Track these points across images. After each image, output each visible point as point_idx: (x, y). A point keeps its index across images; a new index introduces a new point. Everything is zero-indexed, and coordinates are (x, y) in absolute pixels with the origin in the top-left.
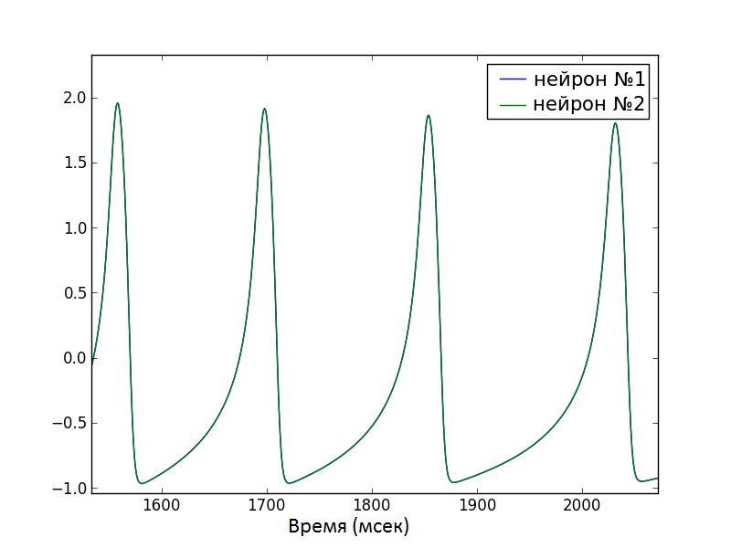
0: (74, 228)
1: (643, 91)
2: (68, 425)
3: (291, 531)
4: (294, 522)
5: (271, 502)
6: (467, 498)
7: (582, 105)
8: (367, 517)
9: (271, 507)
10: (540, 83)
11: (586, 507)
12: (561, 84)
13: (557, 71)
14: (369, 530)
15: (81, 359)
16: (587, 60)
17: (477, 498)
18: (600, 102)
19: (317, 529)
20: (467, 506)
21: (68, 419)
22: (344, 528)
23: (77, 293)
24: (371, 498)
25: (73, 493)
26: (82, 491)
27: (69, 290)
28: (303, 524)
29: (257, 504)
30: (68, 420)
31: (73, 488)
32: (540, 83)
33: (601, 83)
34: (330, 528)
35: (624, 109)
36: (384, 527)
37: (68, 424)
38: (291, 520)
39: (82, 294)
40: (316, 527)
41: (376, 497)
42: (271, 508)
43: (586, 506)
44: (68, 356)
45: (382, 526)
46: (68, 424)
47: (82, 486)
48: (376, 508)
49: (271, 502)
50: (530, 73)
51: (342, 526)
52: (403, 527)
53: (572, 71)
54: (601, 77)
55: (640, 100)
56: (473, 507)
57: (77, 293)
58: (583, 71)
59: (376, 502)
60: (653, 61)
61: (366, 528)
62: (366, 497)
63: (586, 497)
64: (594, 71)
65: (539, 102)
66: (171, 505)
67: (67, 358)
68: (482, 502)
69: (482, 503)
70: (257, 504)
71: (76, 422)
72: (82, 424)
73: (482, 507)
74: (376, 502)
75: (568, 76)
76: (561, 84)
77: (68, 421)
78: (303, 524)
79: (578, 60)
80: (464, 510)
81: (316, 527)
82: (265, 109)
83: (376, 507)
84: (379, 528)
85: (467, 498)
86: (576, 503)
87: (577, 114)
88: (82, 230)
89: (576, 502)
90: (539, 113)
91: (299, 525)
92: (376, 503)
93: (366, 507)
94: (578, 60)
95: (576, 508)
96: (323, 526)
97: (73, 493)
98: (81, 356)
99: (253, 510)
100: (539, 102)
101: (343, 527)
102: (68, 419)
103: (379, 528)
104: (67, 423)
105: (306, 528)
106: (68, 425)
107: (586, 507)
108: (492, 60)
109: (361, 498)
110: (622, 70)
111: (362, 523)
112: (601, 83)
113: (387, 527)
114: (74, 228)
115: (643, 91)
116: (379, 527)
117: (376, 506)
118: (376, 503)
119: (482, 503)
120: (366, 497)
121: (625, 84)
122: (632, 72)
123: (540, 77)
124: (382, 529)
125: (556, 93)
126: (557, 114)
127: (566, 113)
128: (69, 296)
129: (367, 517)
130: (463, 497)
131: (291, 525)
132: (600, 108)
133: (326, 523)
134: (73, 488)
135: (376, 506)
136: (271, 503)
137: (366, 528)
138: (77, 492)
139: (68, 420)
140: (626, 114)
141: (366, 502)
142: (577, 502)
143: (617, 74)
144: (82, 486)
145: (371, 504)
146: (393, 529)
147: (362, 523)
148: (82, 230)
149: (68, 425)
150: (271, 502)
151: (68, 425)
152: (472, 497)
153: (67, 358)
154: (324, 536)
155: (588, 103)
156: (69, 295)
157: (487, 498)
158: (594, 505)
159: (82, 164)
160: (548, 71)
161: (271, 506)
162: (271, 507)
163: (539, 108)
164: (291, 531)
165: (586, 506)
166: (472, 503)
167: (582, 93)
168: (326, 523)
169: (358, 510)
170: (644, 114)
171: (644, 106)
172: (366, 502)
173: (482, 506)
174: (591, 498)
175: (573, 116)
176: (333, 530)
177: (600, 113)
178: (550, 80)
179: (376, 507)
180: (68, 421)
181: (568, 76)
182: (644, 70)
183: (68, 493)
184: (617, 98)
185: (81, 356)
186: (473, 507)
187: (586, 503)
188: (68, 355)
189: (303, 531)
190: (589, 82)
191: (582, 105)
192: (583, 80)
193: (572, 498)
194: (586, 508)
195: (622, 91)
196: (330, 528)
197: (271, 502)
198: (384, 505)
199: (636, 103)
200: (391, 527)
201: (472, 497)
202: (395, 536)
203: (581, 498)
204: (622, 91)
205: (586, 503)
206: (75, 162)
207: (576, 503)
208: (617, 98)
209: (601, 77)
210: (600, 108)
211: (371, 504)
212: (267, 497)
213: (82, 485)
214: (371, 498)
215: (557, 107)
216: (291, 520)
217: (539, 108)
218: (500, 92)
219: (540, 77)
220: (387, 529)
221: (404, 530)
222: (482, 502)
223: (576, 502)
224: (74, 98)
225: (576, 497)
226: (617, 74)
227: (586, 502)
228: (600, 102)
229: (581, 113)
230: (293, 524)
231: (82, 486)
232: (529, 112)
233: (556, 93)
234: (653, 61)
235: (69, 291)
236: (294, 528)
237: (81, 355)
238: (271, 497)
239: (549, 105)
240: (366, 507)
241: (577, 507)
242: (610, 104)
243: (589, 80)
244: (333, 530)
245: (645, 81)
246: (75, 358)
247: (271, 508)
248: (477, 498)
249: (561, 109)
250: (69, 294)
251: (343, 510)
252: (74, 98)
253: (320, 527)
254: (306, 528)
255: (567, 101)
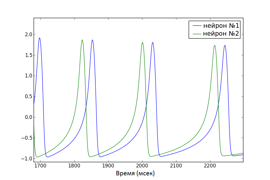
0: (28, 76)
1: (238, 30)
2: (26, 139)
3: (117, 175)
4: (118, 172)
5: (42, 165)
6: (105, 163)
7: (219, 34)
8: (142, 170)
9: (42, 166)
10: (205, 27)
11: (143, 166)
12: (212, 27)
13: (211, 23)
14: (142, 174)
15: (31, 118)
16: (212, 19)
17: (108, 163)
18: (225, 33)
19: (125, 174)
20: (105, 166)
21: (26, 137)
22: (134, 174)
23: (29, 96)
24: (74, 163)
25: (28, 160)
26: (31, 159)
27: (26, 96)
28: (121, 173)
29: (37, 165)
30: (26, 137)
31: (28, 159)
32: (205, 27)
33: (225, 27)
34: (129, 174)
35: (232, 35)
36: (147, 174)
37: (26, 138)
38: (117, 171)
39: (31, 97)
40: (125, 174)
41: (76, 163)
42: (42, 167)
43: (143, 166)
44: (26, 117)
45: (146, 173)
46: (26, 138)
47: (31, 158)
48: (76, 167)
49: (42, 165)
50: (202, 23)
51: (133, 173)
52: (153, 174)
53: (216, 23)
54: (225, 25)
55: (237, 32)
56: (107, 166)
57: (29, 96)
58: (219, 23)
59: (76, 165)
60: (241, 20)
61: (141, 174)
62: (73, 163)
63: (110, 163)
64: (223, 23)
65: (205, 33)
66: (77, 166)
67: (26, 117)
68: (110, 165)
69: (110, 165)
70: (37, 165)
71: (29, 138)
72: (31, 138)
73: (110, 166)
74: (76, 165)
75: (214, 25)
76: (212, 27)
77: (26, 137)
78: (121, 173)
79: (209, 19)
80: (104, 167)
81: (125, 174)
82: (40, 38)
83: (76, 166)
84: (145, 174)
85: (105, 163)
86: (140, 165)
87: (217, 37)
88: (31, 76)
89: (140, 165)
90: (205, 36)
91: (120, 173)
92: (76, 165)
93: (73, 166)
94: (209, 19)
95: (140, 166)
96: (127, 173)
97: (28, 160)
98: (31, 116)
99: (36, 167)
100: (205, 33)
101: (133, 173)
102: (26, 137)
103: (145, 174)
104: (26, 138)
105: (122, 174)
106: (26, 139)
107: (143, 166)
108: (191, 19)
109: (71, 163)
110: (232, 23)
111: (139, 172)
112: (225, 27)
113: (148, 173)
114: (28, 76)
115: (238, 30)
116: (145, 174)
117: (76, 166)
118: (76, 165)
119: (110, 165)
120: (73, 163)
121: (233, 27)
122: (235, 23)
123: (205, 25)
124: (146, 174)
125: (210, 30)
126: (211, 37)
127: (214, 37)
128: (26, 97)
129: (142, 170)
130: (103, 163)
131: (117, 173)
132: (225, 35)
133: (128, 172)
134: (28, 159)
135: (76, 166)
136: (42, 165)
137: (141, 174)
138: (29, 160)
139: (26, 137)
140: (233, 37)
141: (72, 165)
142: (140, 165)
143: (230, 24)
144: (31, 158)
145: (74, 165)
146: (149, 174)
147: (139, 172)
148: (31, 76)
149: (26, 139)
150: (42, 165)
151: (26, 139)
152: (106, 163)
153: (26, 117)
154: (127, 176)
155: (221, 33)
156: (26, 97)
157: (111, 163)
158: (78, 166)
159: (31, 56)
160: (208, 23)
161: (42, 166)
162: (42, 166)
163: (205, 35)
164: (117, 175)
165: (143, 166)
166: (106, 165)
167: (219, 30)
168: (128, 172)
169: (70, 167)
170: (239, 37)
171: (239, 34)
172: (73, 165)
173: (110, 166)
174: (145, 163)
175: (216, 38)
176: (130, 174)
177: (224, 36)
178: (209, 26)
179: (76, 166)
180: (26, 137)
181: (214, 25)
182: (239, 23)
183: (26, 160)
184: (230, 32)
185: (31, 116)
186: (107, 166)
187: (143, 165)
188: (26, 116)
189: (121, 175)
190: (221, 27)
191: (219, 34)
192: (219, 26)
193: (139, 163)
194: (143, 167)
195: (232, 30)
196: (129, 174)
197: (42, 165)
198: (146, 166)
199: (236, 33)
200: (149, 174)
201: (106, 163)
202: (150, 176)
203: (142, 163)
204: (232, 30)
205: (143, 165)
206: (29, 55)
207: (140, 165)
208: (230, 32)
209: (225, 25)
210: (225, 35)
211: (74, 165)
212: (40, 163)
213: (31, 158)
214: (74, 163)
215: (211, 34)
216: (117, 171)
217: (205, 35)
218: (193, 30)
219: (205, 25)
220: (148, 174)
221: (153, 175)
222: (110, 165)
223: (140, 165)
224: (28, 34)
225: (140, 163)
226: (230, 24)
227: (143, 165)
228: (225, 33)
229: (219, 37)
230: (118, 173)
231: (31, 158)
232: (202, 36)
233: (210, 30)
234: (241, 20)
235: (26, 96)
236: (118, 174)
237: (31, 116)
238: (42, 163)
239: (208, 34)
240: (73, 166)
241: (140, 166)
242: (228, 34)
243: (221, 26)
244: (130, 174)
245: (239, 26)
246: (29, 117)
247: (42, 167)
248: (108, 163)
249: (212, 35)
250: (26, 97)
251: (133, 168)
252: (28, 34)
253: (126, 174)
254: (122, 174)
255: (214, 33)
